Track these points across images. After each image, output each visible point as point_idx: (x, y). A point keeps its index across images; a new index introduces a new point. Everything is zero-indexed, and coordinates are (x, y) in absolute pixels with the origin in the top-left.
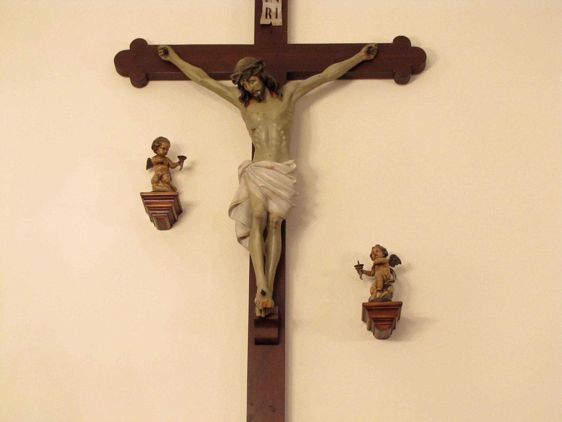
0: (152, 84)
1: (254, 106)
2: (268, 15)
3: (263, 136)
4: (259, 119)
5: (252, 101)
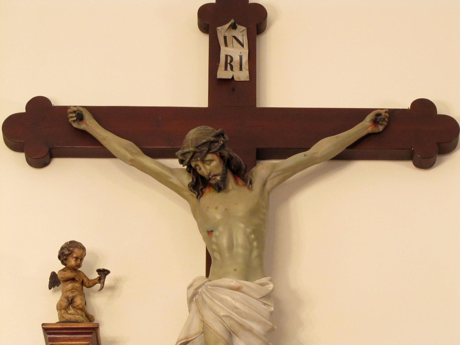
0: (58, 164)
1: (210, 197)
2: (229, 66)
3: (224, 241)
4: (218, 217)
5: (207, 190)
